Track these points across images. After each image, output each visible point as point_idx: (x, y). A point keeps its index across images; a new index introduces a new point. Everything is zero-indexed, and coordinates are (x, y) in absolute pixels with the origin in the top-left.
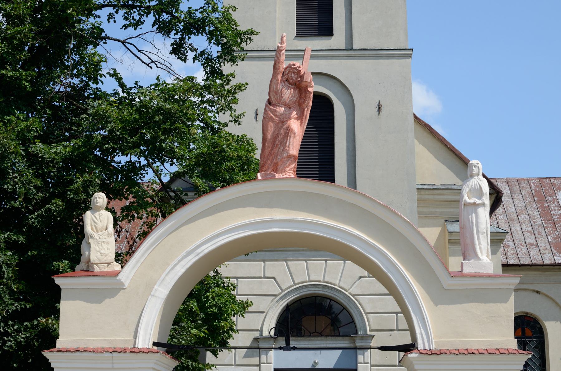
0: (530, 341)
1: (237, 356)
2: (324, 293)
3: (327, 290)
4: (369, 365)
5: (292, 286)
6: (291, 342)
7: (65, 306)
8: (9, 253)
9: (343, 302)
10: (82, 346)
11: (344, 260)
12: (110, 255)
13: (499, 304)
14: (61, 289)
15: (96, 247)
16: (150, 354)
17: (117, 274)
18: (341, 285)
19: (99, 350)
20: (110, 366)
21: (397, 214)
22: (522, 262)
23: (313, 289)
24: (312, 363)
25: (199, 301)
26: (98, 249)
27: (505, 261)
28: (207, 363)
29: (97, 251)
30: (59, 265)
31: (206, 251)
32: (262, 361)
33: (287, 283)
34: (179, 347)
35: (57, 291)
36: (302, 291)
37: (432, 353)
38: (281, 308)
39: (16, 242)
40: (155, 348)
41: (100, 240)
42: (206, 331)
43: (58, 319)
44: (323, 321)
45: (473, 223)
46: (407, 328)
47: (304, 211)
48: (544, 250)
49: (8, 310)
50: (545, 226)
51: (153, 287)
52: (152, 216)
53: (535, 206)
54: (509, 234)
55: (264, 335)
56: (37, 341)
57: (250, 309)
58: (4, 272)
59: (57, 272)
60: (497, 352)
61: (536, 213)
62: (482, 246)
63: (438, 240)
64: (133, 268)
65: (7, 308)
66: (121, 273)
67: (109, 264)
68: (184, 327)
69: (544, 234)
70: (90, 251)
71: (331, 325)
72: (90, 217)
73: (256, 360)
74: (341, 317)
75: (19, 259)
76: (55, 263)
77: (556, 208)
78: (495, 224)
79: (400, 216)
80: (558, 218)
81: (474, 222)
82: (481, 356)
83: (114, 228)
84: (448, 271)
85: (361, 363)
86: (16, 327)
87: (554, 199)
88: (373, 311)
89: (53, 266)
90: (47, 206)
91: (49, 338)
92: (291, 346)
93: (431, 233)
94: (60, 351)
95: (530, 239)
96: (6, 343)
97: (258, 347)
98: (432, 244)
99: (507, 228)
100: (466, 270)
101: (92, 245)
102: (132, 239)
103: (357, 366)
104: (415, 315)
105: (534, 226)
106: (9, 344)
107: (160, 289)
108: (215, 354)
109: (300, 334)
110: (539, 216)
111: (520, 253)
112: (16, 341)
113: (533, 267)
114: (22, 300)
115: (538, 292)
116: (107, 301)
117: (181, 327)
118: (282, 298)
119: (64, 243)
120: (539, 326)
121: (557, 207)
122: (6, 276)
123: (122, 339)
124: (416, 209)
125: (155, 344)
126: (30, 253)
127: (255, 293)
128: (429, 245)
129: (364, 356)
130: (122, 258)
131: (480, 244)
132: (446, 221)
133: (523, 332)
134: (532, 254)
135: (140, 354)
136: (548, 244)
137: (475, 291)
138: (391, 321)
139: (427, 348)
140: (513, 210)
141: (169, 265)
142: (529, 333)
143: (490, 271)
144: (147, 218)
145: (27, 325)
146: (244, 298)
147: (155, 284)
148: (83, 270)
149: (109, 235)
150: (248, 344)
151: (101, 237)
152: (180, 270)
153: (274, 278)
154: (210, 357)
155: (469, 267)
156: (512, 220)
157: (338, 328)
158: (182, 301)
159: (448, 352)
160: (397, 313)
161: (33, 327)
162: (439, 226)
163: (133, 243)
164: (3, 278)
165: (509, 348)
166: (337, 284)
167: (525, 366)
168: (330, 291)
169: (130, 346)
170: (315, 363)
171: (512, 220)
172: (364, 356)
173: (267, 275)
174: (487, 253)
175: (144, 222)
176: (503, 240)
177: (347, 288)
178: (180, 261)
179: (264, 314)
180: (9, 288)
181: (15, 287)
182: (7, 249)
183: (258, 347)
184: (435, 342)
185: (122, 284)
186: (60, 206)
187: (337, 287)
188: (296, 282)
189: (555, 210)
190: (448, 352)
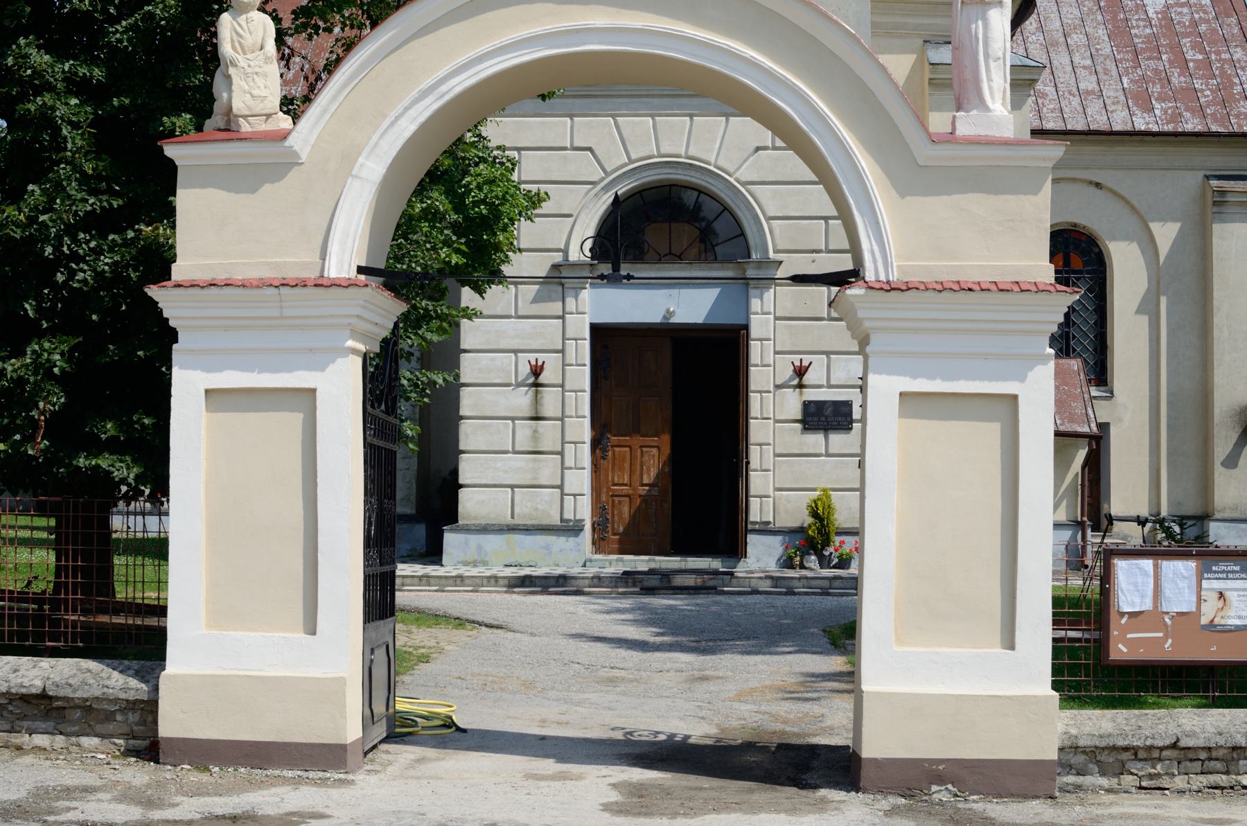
0: (1078, 279)
2: (688, 178)
3: (693, 173)
5: (626, 165)
6: (622, 266)
7: (186, 200)
8: (74, 101)
9: (723, 196)
10: (221, 276)
11: (727, 115)
12: (271, 98)
13: (1022, 197)
14: (175, 168)
15: (243, 84)
16: (351, 290)
17: (284, 136)
18: (721, 163)
19: (255, 283)
20: (276, 313)
21: (830, 19)
22: (1069, 127)
23: (666, 171)
24: (663, 313)
25: (449, 192)
26: (247, 87)
27: (1036, 124)
28: (463, 305)
29: (245, 92)
30: (174, 124)
31: (458, 89)
32: (568, 310)
33: (616, 159)
34: (409, 276)
35: (169, 171)
36: (644, 174)
37: (891, 288)
38: (604, 208)
39: (86, 80)
40: (362, 277)
41: (249, 70)
42: (463, 248)
43: (173, 227)
44: (685, 233)
45: (977, 39)
46: (846, 246)
47: (649, 11)
48: (1113, 103)
49: (76, 211)
50: (1118, 57)
51: (356, 160)
52: (352, 27)
53: (1100, 17)
54: (1048, 70)
55: (571, 259)
56: (135, 270)
57: (546, 207)
58: (66, 137)
59: (170, 134)
60: (1016, 288)
61: (1102, 32)
62: (994, 85)
63: (909, 78)
64: (317, 122)
65: (74, 208)
66: (294, 134)
67: (268, 116)
68: (417, 242)
69: (1114, 73)
70: (230, 91)
71: (701, 242)
72: (229, 26)
73: (556, 307)
74: (717, 226)
75: (95, 113)
76: (165, 119)
77: (1142, 23)
78: (1021, 51)
79: (836, 22)
80: (1143, 42)
81: (980, 36)
82: (985, 294)
83: (279, 49)
84: (926, 130)
85: (757, 313)
86: (93, 244)
87: (1137, 5)
89: (162, 124)
90: (146, 8)
91: (159, 262)
92: (623, 273)
93: (900, 65)
94: (180, 286)
95: (1088, 83)
96: (75, 275)
97: (560, 279)
98: (901, 83)
99: (1045, 61)
100: (962, 130)
101: (236, 80)
102: (313, 72)
103: (748, 318)
104: (862, 215)
105: (1096, 58)
106: (80, 276)
107: (368, 163)
108: (480, 291)
109: (639, 255)
110: (1106, 38)
111: (1066, 110)
112: (94, 270)
113: (1090, 137)
114: (103, 193)
115: (1098, 185)
116: (267, 188)
117: (412, 242)
118: (606, 189)
119: (182, 77)
120: (1096, 250)
121: (1144, 20)
122: (69, 146)
123: (296, 260)
124: (867, 17)
125: (361, 270)
126: (115, 102)
127: (554, 178)
128: (892, 80)
129: (762, 299)
130: (292, 106)
131: (990, 80)
132: (925, 42)
133: (1067, 262)
134: (1089, 111)
135: (334, 290)
136: (1121, 93)
137: (981, 171)
138: (815, 234)
139: (883, 278)
140: (1058, 24)
141: (385, 116)
142: (1077, 262)
143: (1008, 133)
144: (343, 29)
145: (113, 240)
146: (533, 188)
147: (359, 154)
148: (219, 130)
149: (267, 60)
151: (252, 64)
152: (408, 127)
153: (590, 149)
154: (468, 296)
155: (968, 125)
156: (1055, 44)
157: (713, 247)
158: (414, 185)
159: (922, 287)
160: (826, 219)
161: (127, 243)
162: (912, 52)
163: (316, 80)
164: (65, 149)
165: (1038, 280)
166: (713, 162)
167: (1067, 315)
168: (698, 175)
169: (312, 274)
170: (669, 314)
171: (1055, 44)
172: (762, 299)
173: (576, 144)
174: (1004, 98)
175: (337, 40)
176: (1035, 81)
177: (731, 170)
178: (407, 109)
179: (572, 220)
180: (77, 168)
181: (88, 168)
182: (69, 92)
183: (560, 279)
184: (898, 266)
185: (296, 154)
186: (171, 8)
187: (711, 168)
188: (634, 156)
189: (1138, 27)
190: (922, 287)
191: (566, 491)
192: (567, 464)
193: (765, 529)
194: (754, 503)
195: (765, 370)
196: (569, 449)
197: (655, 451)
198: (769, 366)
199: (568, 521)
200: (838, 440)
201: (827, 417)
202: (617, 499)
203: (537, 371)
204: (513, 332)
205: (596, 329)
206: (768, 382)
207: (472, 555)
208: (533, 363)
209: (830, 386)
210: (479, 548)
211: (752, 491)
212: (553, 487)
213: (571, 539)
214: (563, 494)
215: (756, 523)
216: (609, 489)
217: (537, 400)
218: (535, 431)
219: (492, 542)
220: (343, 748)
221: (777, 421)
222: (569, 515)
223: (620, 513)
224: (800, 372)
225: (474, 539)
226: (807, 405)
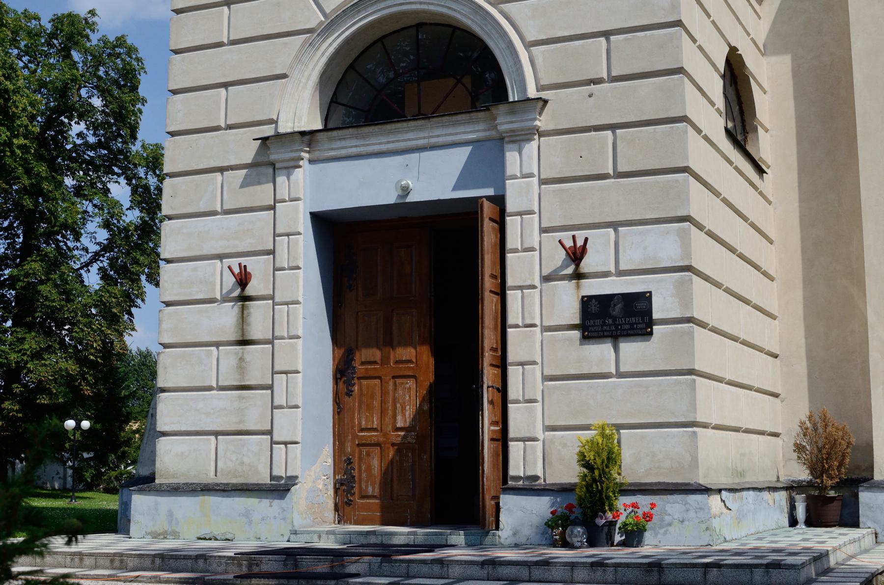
1: (225, 189)
4: (535, 180)
85: (514, 177)
88: (543, 37)
150: (248, 158)
193: (531, 487)
195: (528, 254)
197: (411, 383)
198: (532, 249)
199: (280, 478)
200: (633, 351)
201: (614, 319)
202: (364, 450)
203: (243, 279)
204: (218, 233)
205: (320, 220)
206: (531, 273)
207: (161, 524)
208: (237, 270)
209: (621, 273)
210: (170, 514)
213: (276, 502)
214: (273, 442)
215: (518, 478)
216: (355, 436)
217: (243, 319)
218: (241, 359)
219: (185, 505)
222: (279, 471)
223: (369, 469)
224: (576, 255)
225: (165, 502)
226: (586, 302)
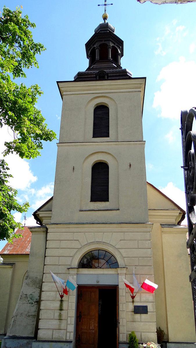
191: (68, 331)
192: (68, 323)
194: (121, 336)
196: (69, 319)
211: (120, 332)
212: (64, 330)
214: (67, 332)
218: (60, 313)
220: (59, 324)
221: (127, 312)
225: (41, 343)
226: (136, 307)
